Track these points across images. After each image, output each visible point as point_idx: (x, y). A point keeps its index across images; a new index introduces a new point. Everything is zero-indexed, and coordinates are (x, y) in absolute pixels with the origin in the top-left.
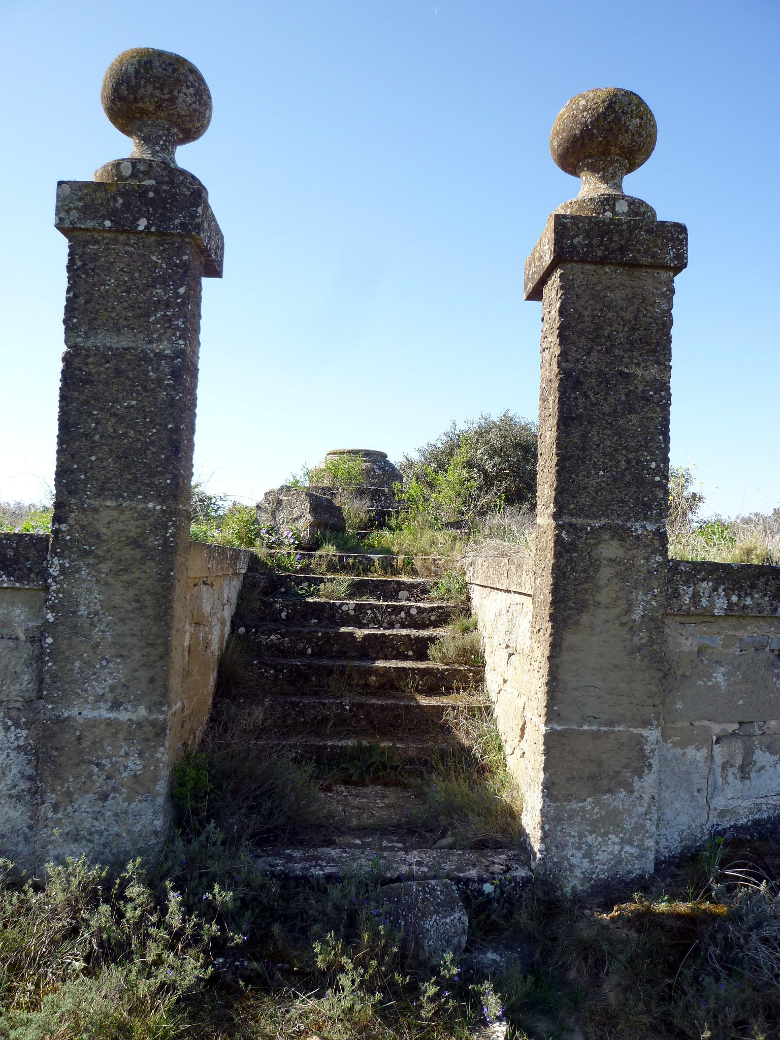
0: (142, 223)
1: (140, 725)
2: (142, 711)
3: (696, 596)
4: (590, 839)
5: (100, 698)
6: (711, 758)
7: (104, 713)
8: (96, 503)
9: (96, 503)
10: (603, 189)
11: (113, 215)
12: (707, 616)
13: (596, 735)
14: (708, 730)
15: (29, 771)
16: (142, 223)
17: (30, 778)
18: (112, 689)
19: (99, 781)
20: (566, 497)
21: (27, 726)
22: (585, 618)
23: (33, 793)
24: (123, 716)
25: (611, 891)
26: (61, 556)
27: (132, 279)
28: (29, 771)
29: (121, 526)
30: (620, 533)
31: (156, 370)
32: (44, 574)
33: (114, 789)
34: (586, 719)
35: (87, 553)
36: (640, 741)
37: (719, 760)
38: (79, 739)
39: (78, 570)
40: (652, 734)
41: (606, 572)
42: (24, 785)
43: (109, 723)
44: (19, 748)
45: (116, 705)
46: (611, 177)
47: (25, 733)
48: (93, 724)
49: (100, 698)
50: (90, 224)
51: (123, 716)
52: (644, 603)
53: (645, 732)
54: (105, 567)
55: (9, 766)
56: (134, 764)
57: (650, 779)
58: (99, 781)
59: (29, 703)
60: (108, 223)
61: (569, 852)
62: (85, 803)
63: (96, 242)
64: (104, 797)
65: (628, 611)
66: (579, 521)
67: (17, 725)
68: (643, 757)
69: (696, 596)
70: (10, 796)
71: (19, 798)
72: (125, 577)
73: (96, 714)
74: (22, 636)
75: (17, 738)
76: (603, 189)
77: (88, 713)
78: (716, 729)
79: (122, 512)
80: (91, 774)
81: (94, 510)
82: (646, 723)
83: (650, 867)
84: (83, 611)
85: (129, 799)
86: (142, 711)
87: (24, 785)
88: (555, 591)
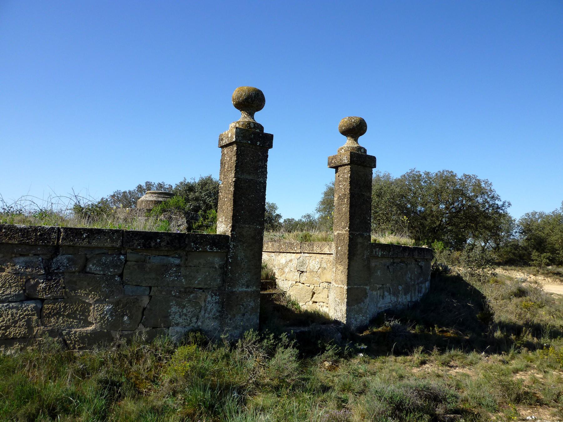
0: (258, 143)
1: (254, 292)
2: (255, 288)
3: (376, 252)
4: (356, 316)
5: (243, 285)
6: (377, 294)
7: (244, 289)
8: (243, 226)
9: (243, 226)
10: (248, 119)
11: (251, 139)
12: (377, 257)
13: (357, 288)
14: (376, 287)
15: (220, 309)
16: (258, 143)
17: (220, 312)
18: (247, 282)
19: (242, 310)
20: (167, 239)
21: (219, 295)
22: (355, 258)
23: (221, 316)
24: (249, 290)
25: (362, 329)
26: (233, 241)
27: (254, 159)
28: (220, 309)
29: (250, 233)
30: (362, 235)
31: (259, 186)
32: (228, 247)
33: (247, 312)
34: (355, 284)
35: (241, 241)
36: (366, 289)
37: (379, 294)
38: (237, 297)
39: (238, 246)
40: (368, 288)
41: (359, 246)
42: (218, 314)
43: (246, 292)
44: (216, 303)
45: (248, 287)
46: (251, 115)
47: (218, 297)
48: (241, 292)
49: (243, 285)
50: (245, 141)
51: (249, 290)
52: (367, 253)
53: (366, 287)
54: (245, 245)
55: (213, 309)
56: (252, 304)
57: (368, 299)
58: (242, 310)
59: (219, 288)
60: (249, 142)
61: (352, 319)
62: (238, 317)
63: (244, 146)
64: (244, 315)
65: (363, 256)
66: (354, 232)
67: (216, 295)
68: (366, 294)
69: (376, 252)
70: (213, 318)
71: (216, 318)
72: (250, 248)
73: (242, 289)
74: (217, 267)
75: (216, 299)
76: (248, 119)
77: (240, 289)
78: (378, 286)
79: (250, 228)
80: (240, 308)
81: (243, 228)
82: (367, 285)
83: (368, 322)
84: (239, 258)
85: (250, 315)
86: (255, 288)
87: (218, 314)
88: (349, 251)
